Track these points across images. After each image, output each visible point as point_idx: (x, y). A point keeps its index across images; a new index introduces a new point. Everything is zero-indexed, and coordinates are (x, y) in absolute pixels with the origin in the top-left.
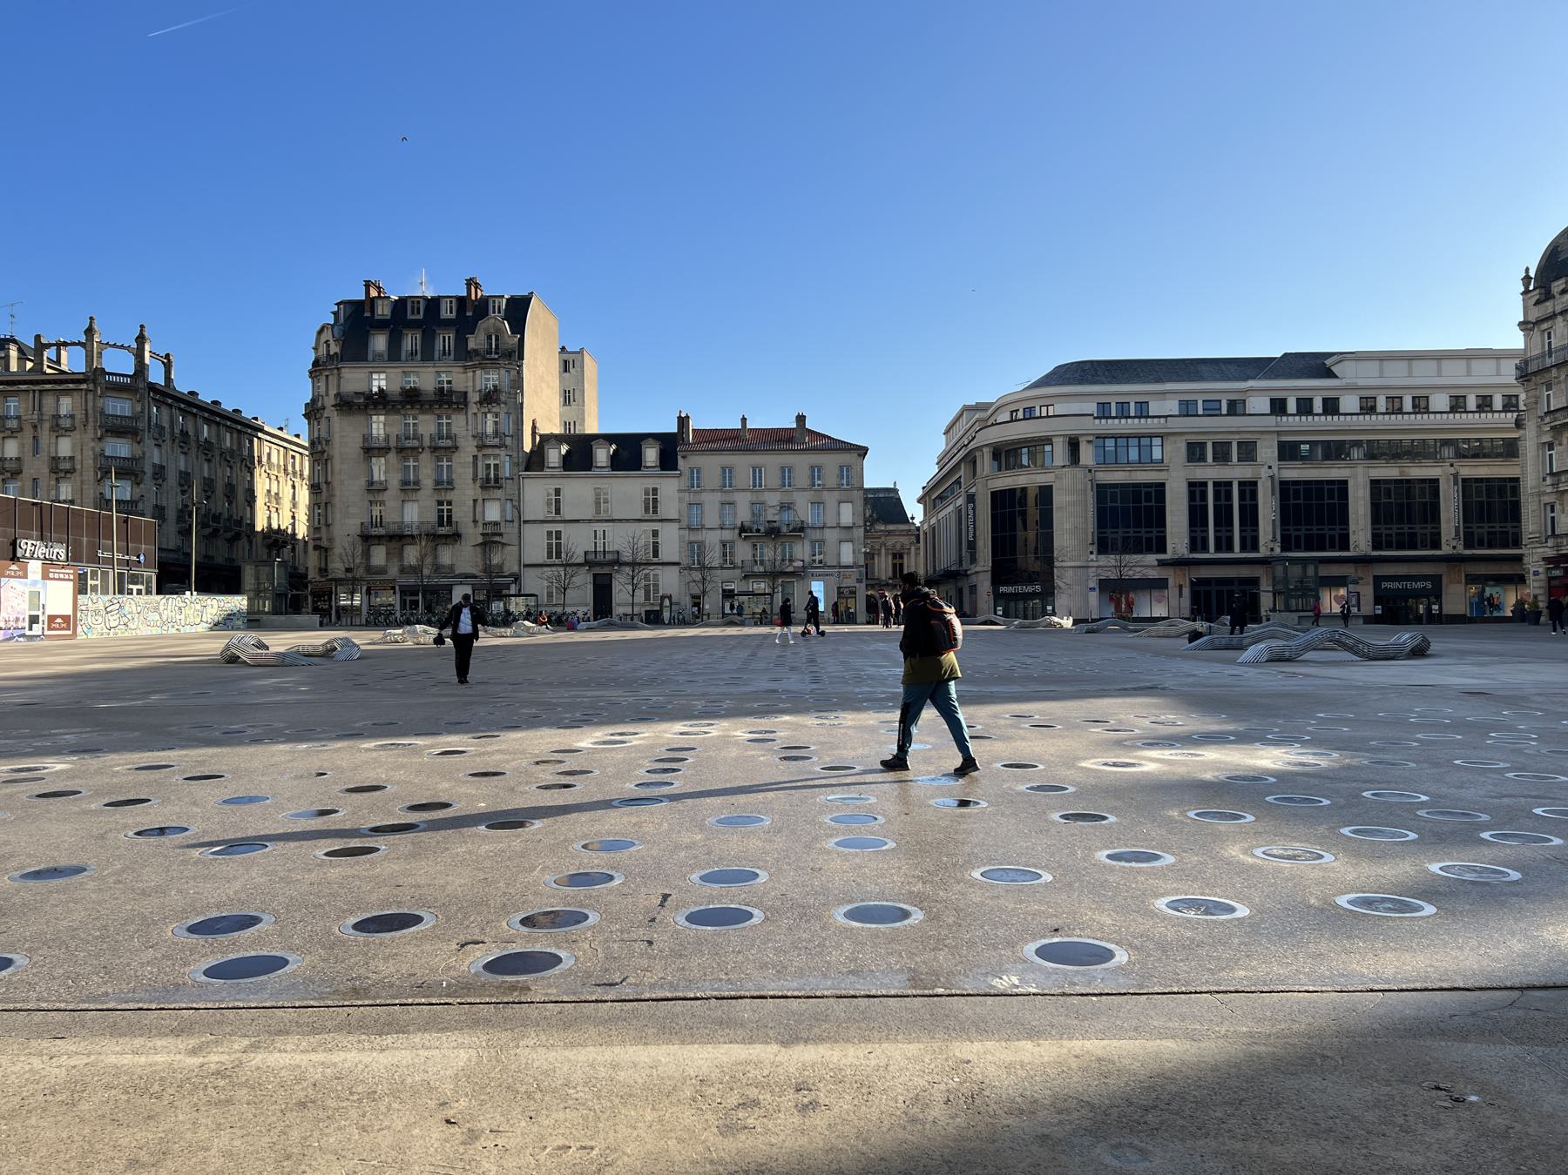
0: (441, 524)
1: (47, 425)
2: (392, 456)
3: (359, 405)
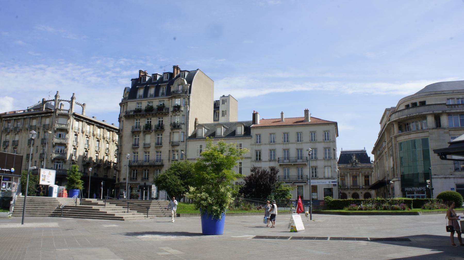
3: (131, 115)
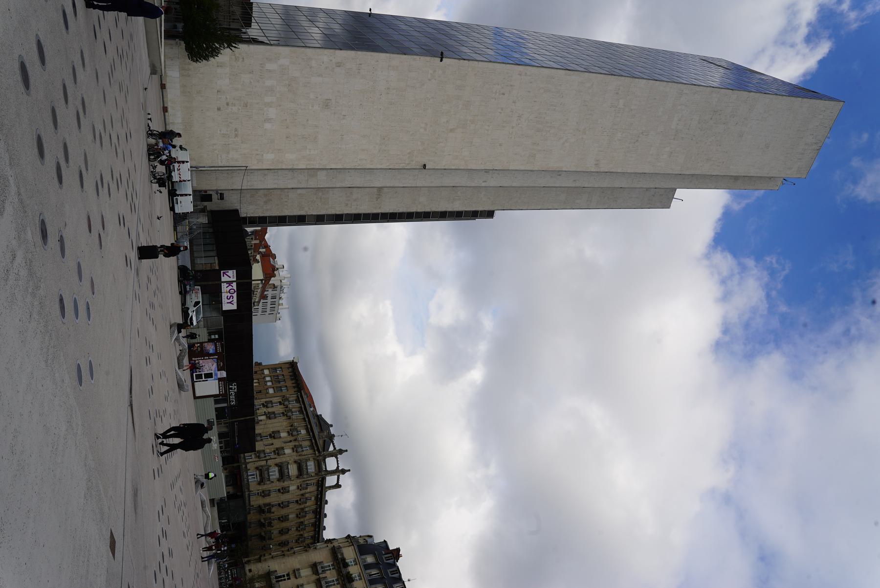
0: (277, 577)
1: (297, 444)
2: (315, 577)
